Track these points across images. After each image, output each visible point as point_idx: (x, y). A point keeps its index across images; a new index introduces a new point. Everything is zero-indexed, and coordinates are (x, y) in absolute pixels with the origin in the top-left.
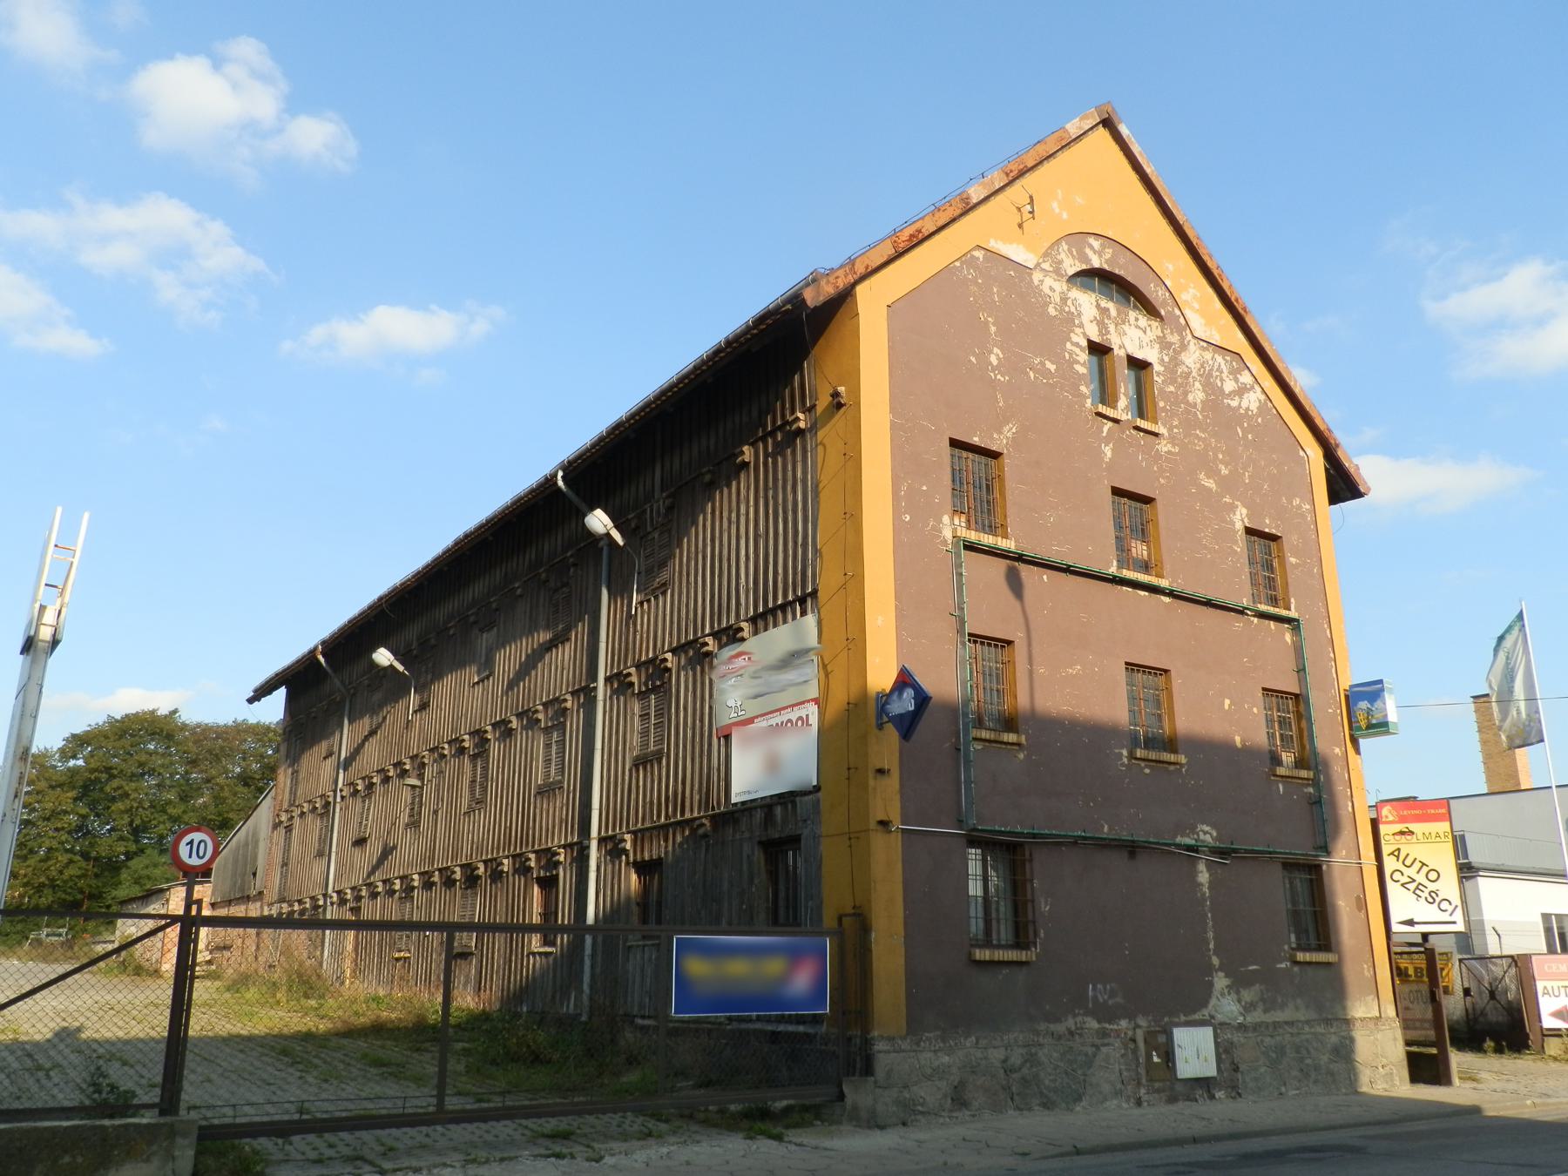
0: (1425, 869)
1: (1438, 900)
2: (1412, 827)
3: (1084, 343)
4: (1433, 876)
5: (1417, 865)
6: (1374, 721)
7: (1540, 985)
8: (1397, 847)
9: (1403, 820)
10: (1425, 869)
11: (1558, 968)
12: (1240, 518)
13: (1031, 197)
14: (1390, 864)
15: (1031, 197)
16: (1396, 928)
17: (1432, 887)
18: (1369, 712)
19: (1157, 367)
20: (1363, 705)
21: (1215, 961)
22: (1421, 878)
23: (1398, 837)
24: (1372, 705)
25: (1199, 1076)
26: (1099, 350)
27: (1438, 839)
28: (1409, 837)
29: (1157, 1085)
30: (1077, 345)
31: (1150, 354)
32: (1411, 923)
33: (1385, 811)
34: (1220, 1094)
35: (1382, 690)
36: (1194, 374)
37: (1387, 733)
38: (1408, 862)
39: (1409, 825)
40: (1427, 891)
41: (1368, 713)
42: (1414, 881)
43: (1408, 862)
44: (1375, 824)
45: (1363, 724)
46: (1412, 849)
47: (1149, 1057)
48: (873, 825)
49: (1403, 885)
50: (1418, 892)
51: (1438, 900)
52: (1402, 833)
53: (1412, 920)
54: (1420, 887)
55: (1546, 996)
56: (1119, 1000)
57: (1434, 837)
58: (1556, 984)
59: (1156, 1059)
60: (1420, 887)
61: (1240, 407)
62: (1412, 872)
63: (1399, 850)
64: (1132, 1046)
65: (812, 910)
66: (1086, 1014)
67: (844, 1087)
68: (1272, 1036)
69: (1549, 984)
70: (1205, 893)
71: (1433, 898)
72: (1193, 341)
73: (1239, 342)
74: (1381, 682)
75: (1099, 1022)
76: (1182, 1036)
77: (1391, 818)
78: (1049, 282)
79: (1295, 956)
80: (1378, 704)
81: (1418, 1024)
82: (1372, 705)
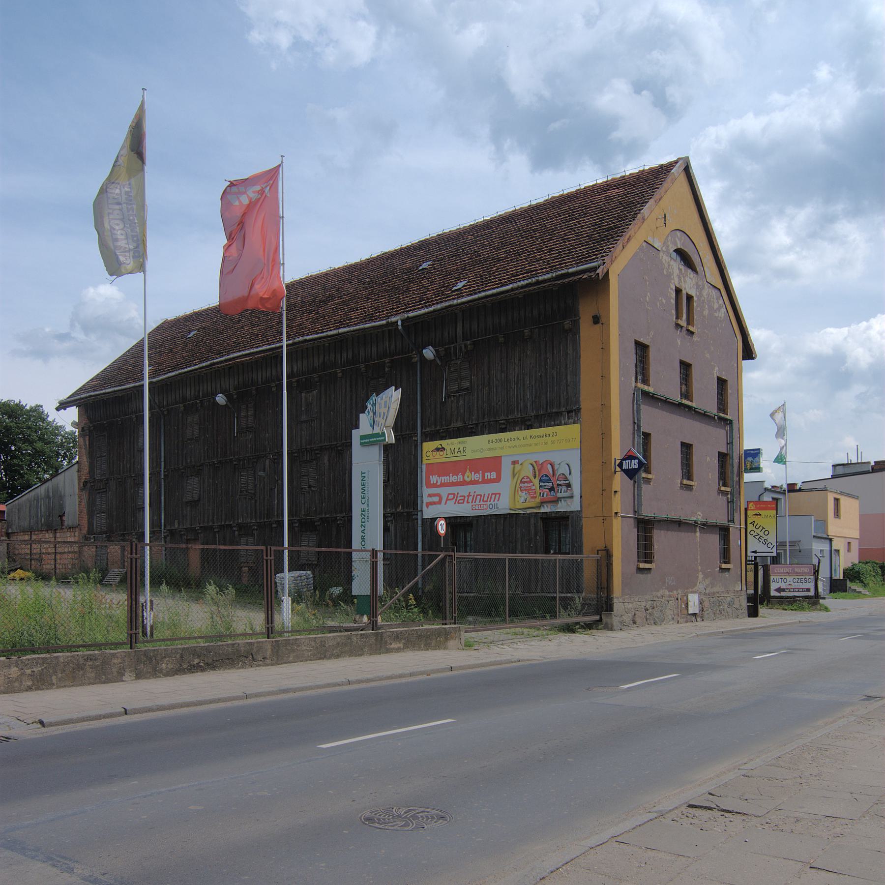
0: (764, 530)
1: (767, 543)
2: (760, 512)
3: (674, 288)
4: (766, 533)
5: (761, 528)
6: (754, 467)
7: (772, 578)
8: (754, 520)
9: (757, 509)
10: (764, 530)
11: (780, 570)
12: (716, 373)
13: (665, 215)
14: (750, 527)
15: (665, 215)
16: (749, 554)
17: (766, 537)
18: (752, 462)
19: (695, 299)
20: (750, 459)
21: (700, 568)
22: (761, 534)
23: (754, 516)
24: (754, 459)
25: (80, 687)
26: (678, 291)
27: (770, 518)
28: (441, 453)
29: (683, 616)
30: (672, 289)
31: (692, 292)
32: (755, 552)
33: (751, 505)
34: (698, 619)
35: (759, 453)
36: (706, 301)
37: (759, 472)
38: (757, 527)
39: (759, 511)
40: (763, 539)
41: (751, 463)
42: (759, 535)
43: (757, 527)
44: (746, 510)
45: (749, 467)
46: (758, 520)
47: (681, 605)
48: (613, 514)
49: (754, 536)
50: (760, 539)
51: (767, 543)
52: (756, 514)
53: (756, 551)
54: (761, 537)
55: (774, 582)
56: (674, 583)
57: (456, 452)
58: (778, 577)
59: (683, 606)
60: (761, 537)
61: (718, 316)
62: (758, 531)
63: (754, 522)
64: (677, 601)
65: (576, 548)
66: (665, 589)
67: (602, 616)
68: (713, 598)
69: (775, 577)
70: (698, 541)
71: (765, 542)
72: (707, 283)
73: (720, 285)
74: (759, 449)
75: (669, 592)
76: (690, 596)
77: (753, 508)
78: (665, 256)
79: (721, 566)
80: (757, 459)
81: (791, 590)
82: (754, 459)
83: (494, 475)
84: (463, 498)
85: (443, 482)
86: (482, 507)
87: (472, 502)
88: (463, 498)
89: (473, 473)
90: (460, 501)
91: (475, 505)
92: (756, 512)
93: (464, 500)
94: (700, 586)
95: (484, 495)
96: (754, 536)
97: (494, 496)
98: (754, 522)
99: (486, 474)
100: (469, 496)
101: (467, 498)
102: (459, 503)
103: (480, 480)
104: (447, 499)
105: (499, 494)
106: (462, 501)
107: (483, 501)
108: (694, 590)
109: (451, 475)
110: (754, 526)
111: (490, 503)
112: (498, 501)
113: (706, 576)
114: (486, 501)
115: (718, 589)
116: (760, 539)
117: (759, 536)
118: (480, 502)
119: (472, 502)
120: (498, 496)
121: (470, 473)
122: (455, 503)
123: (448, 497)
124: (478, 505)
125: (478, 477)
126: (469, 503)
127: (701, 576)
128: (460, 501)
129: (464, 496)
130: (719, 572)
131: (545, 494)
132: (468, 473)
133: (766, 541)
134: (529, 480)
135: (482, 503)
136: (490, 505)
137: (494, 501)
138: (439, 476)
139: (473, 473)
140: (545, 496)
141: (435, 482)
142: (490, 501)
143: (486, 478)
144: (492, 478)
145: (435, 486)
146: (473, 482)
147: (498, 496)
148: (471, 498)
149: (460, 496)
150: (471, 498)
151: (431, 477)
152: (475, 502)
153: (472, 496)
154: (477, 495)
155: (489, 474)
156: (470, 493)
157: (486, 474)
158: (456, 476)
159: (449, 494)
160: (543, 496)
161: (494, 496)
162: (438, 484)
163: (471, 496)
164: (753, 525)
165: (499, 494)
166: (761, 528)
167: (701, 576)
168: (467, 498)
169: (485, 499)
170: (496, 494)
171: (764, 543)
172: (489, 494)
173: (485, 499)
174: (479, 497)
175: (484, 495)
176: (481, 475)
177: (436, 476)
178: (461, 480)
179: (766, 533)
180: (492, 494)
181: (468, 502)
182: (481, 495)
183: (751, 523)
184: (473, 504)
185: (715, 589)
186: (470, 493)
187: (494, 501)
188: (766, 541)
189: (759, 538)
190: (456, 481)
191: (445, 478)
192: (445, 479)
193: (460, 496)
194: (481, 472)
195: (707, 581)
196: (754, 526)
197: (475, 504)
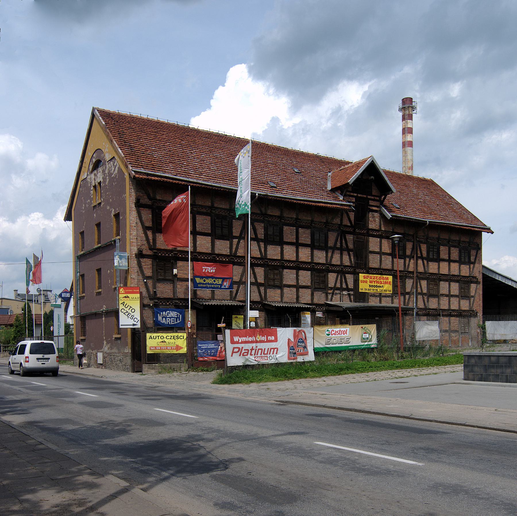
0: (131, 308)
2: (129, 295)
4: (133, 311)
5: (129, 307)
9: (126, 293)
10: (131, 308)
17: (132, 314)
22: (130, 311)
23: (124, 298)
28: (127, 298)
38: (126, 307)
42: (127, 312)
43: (126, 307)
46: (127, 302)
49: (124, 313)
50: (128, 315)
52: (125, 297)
54: (129, 314)
60: (129, 314)
62: (127, 309)
63: (124, 302)
68: (111, 356)
71: (132, 318)
77: (123, 292)
83: (273, 338)
84: (247, 351)
85: (243, 340)
86: (263, 358)
87: (255, 355)
88: (247, 351)
89: (261, 336)
90: (245, 354)
91: (258, 357)
92: (125, 295)
93: (248, 353)
94: (106, 348)
95: (265, 349)
96: (124, 313)
97: (272, 350)
98: (124, 302)
99: (269, 337)
100: (252, 349)
101: (250, 351)
102: (243, 355)
103: (265, 340)
104: (233, 352)
105: (277, 349)
106: (246, 354)
107: (264, 354)
108: (102, 350)
109: (248, 337)
110: (124, 305)
111: (270, 355)
112: (276, 353)
113: (108, 343)
114: (266, 354)
115: (115, 350)
116: (128, 315)
117: (128, 313)
118: (261, 354)
119: (255, 355)
120: (276, 350)
121: (259, 336)
122: (240, 355)
123: (233, 350)
124: (260, 357)
125: (264, 338)
126: (252, 355)
127: (105, 342)
128: (245, 354)
129: (248, 350)
130: (115, 340)
131: (302, 350)
132: (258, 336)
133: (133, 316)
134: (302, 341)
135: (263, 355)
136: (270, 357)
137: (273, 354)
138: (240, 337)
139: (261, 336)
140: (302, 352)
141: (237, 341)
142: (270, 354)
143: (269, 339)
144: (272, 339)
145: (238, 343)
146: (261, 342)
147: (276, 350)
148: (253, 352)
149: (245, 350)
150: (253, 352)
151: (234, 337)
152: (257, 355)
153: (254, 350)
154: (259, 349)
155: (270, 337)
156: (253, 347)
157: (269, 337)
158: (263, 340)
159: (234, 348)
160: (300, 351)
161: (272, 350)
162: (240, 341)
163: (254, 349)
164: (124, 305)
165: (277, 349)
166: (129, 307)
167: (105, 342)
168: (250, 351)
169: (266, 352)
170: (274, 349)
171: (132, 318)
172: (268, 349)
173: (266, 352)
174: (260, 351)
175: (265, 349)
176: (266, 337)
177: (238, 337)
178: (254, 340)
179: (133, 311)
180: (271, 349)
181: (251, 355)
182: (262, 349)
183: (122, 303)
184: (256, 356)
185: (113, 351)
186: (253, 347)
187: (273, 354)
188: (133, 316)
189: (128, 314)
190: (251, 340)
191: (244, 338)
192: (244, 339)
193: (245, 350)
194: (265, 336)
195: (109, 345)
196: (124, 305)
197: (257, 356)
